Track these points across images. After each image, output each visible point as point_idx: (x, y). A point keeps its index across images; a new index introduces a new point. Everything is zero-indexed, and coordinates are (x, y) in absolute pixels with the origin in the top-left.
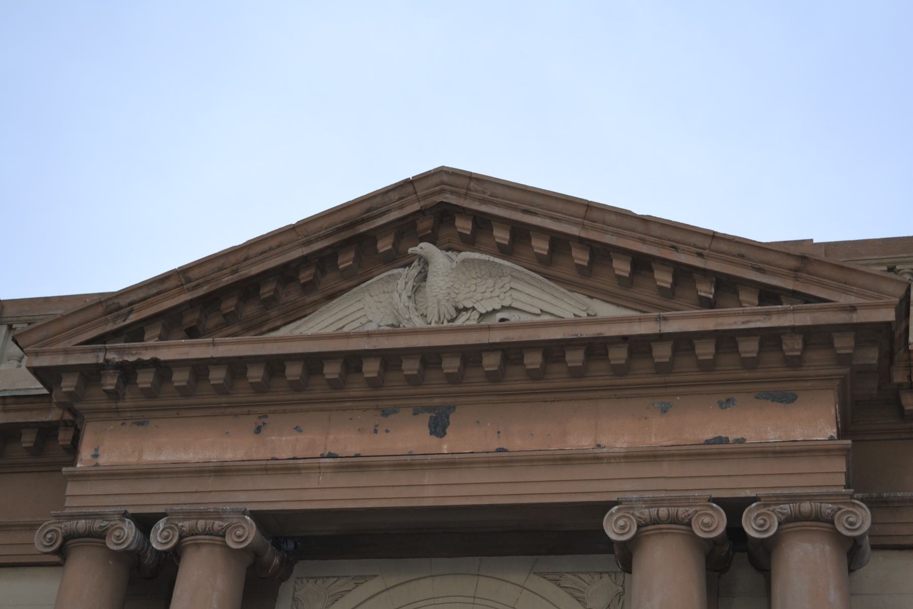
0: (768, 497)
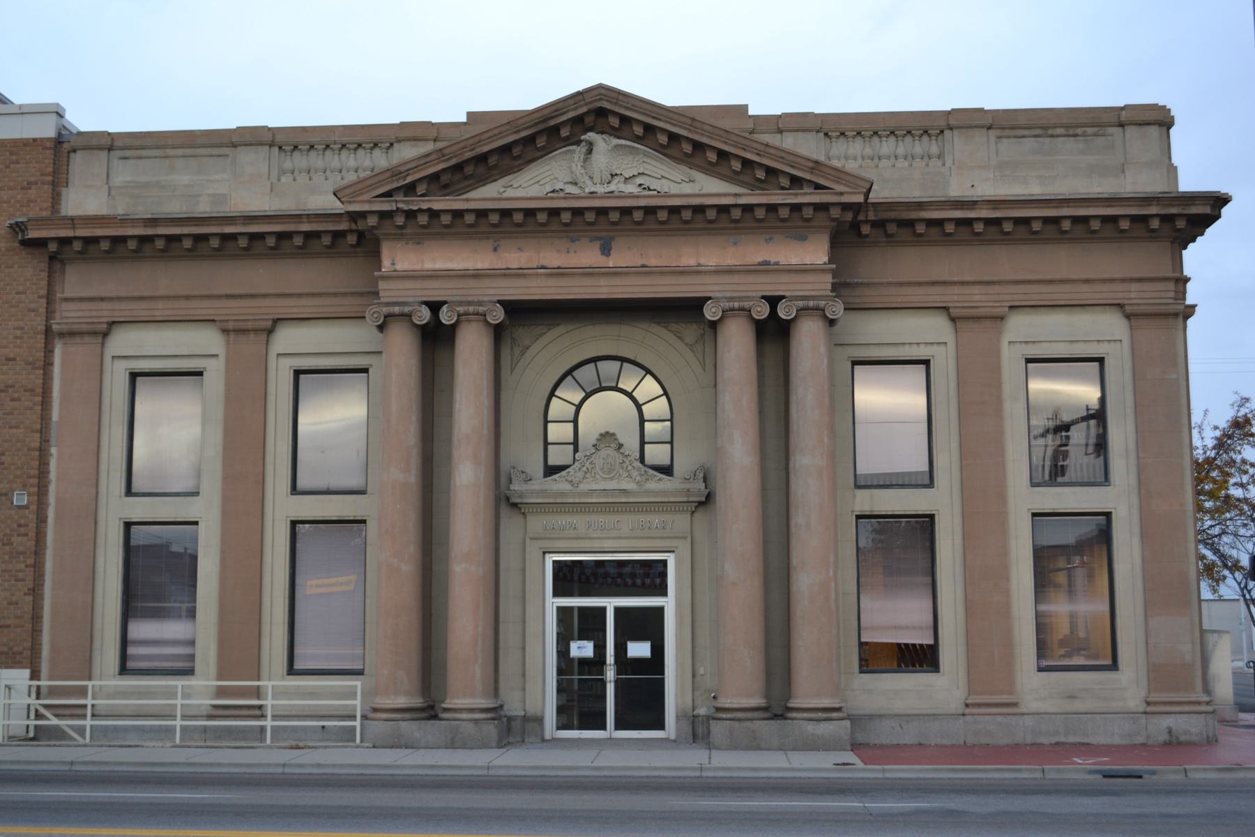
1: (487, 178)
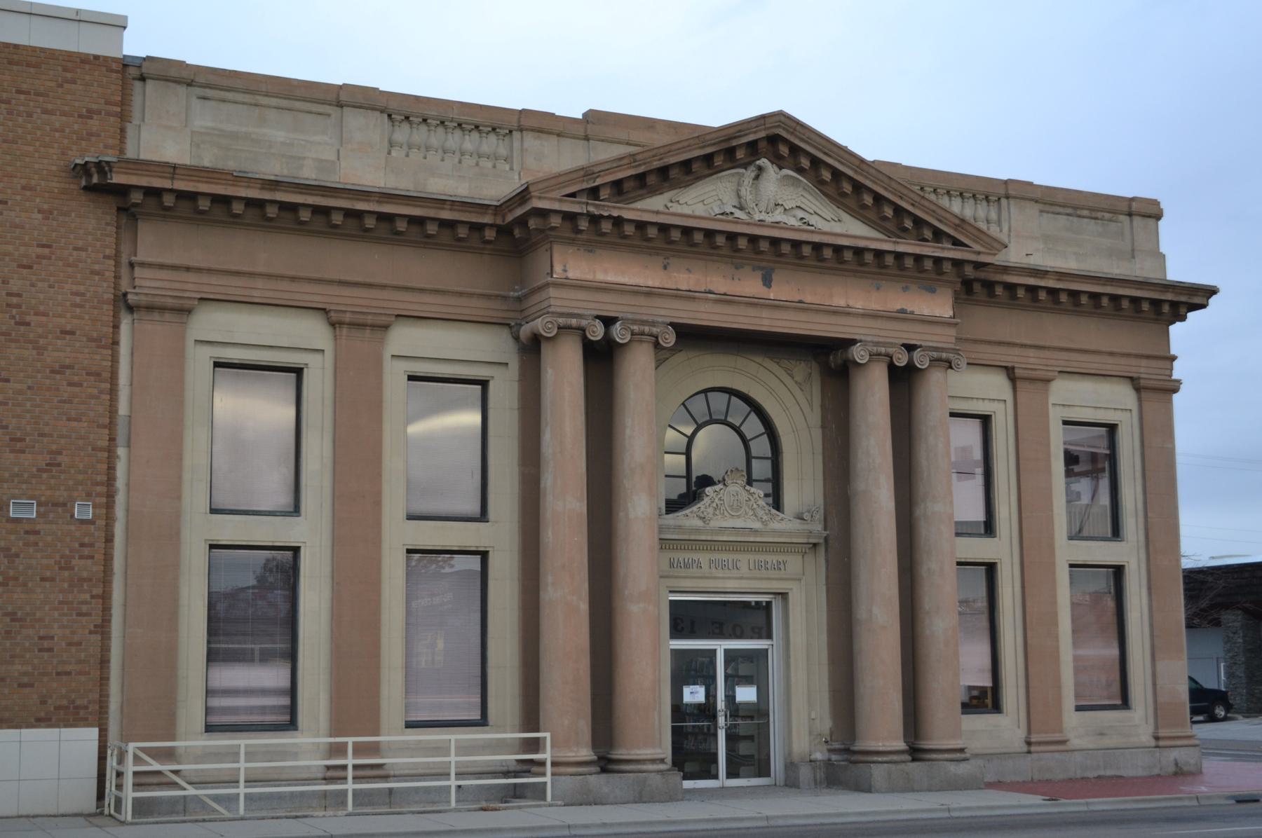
0: (926, 347)
1: (656, 191)
